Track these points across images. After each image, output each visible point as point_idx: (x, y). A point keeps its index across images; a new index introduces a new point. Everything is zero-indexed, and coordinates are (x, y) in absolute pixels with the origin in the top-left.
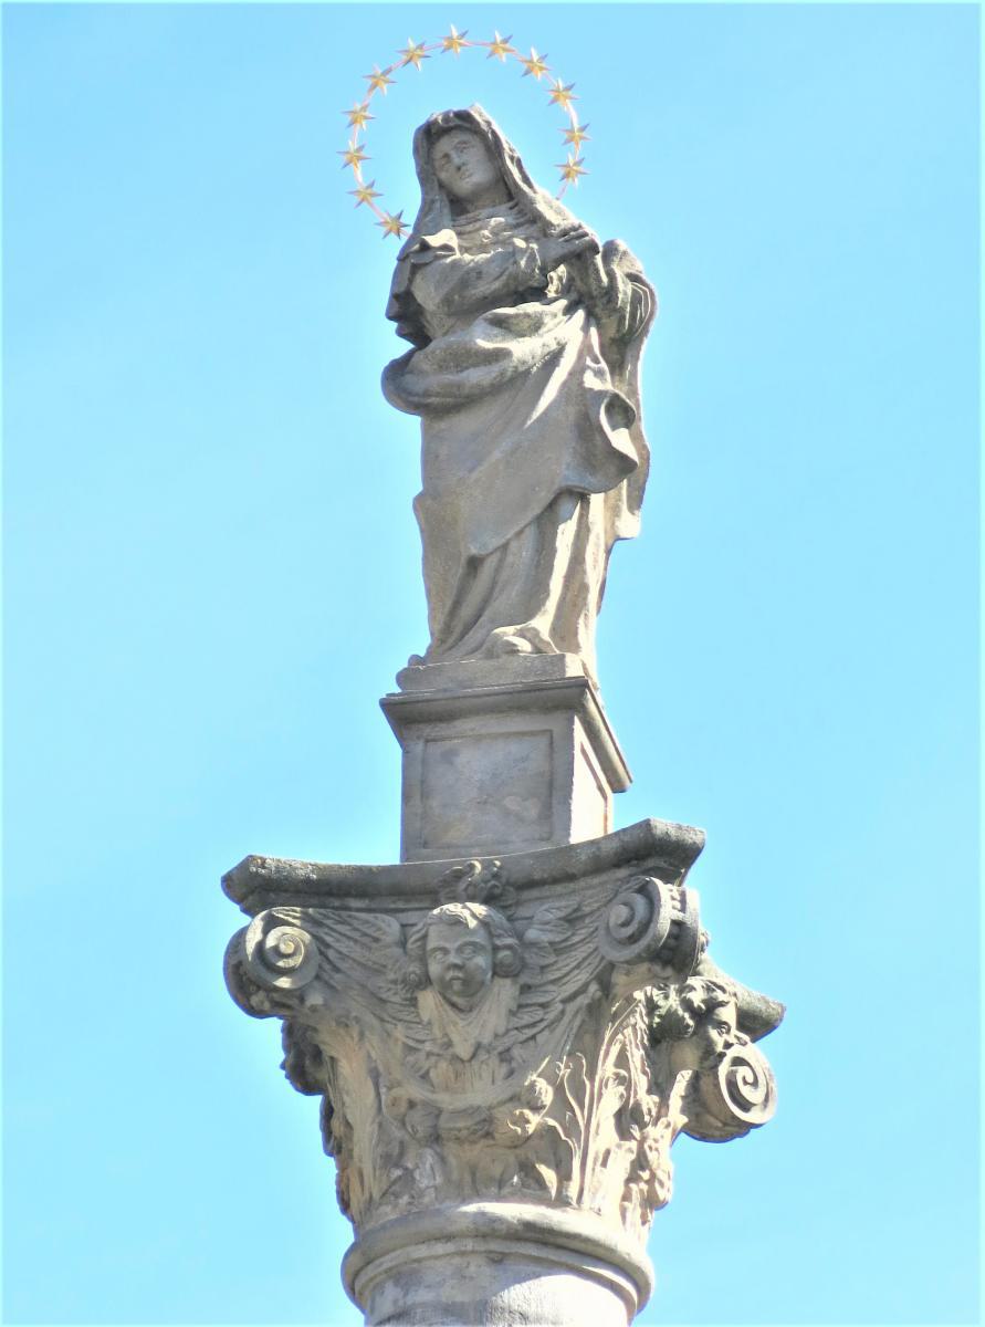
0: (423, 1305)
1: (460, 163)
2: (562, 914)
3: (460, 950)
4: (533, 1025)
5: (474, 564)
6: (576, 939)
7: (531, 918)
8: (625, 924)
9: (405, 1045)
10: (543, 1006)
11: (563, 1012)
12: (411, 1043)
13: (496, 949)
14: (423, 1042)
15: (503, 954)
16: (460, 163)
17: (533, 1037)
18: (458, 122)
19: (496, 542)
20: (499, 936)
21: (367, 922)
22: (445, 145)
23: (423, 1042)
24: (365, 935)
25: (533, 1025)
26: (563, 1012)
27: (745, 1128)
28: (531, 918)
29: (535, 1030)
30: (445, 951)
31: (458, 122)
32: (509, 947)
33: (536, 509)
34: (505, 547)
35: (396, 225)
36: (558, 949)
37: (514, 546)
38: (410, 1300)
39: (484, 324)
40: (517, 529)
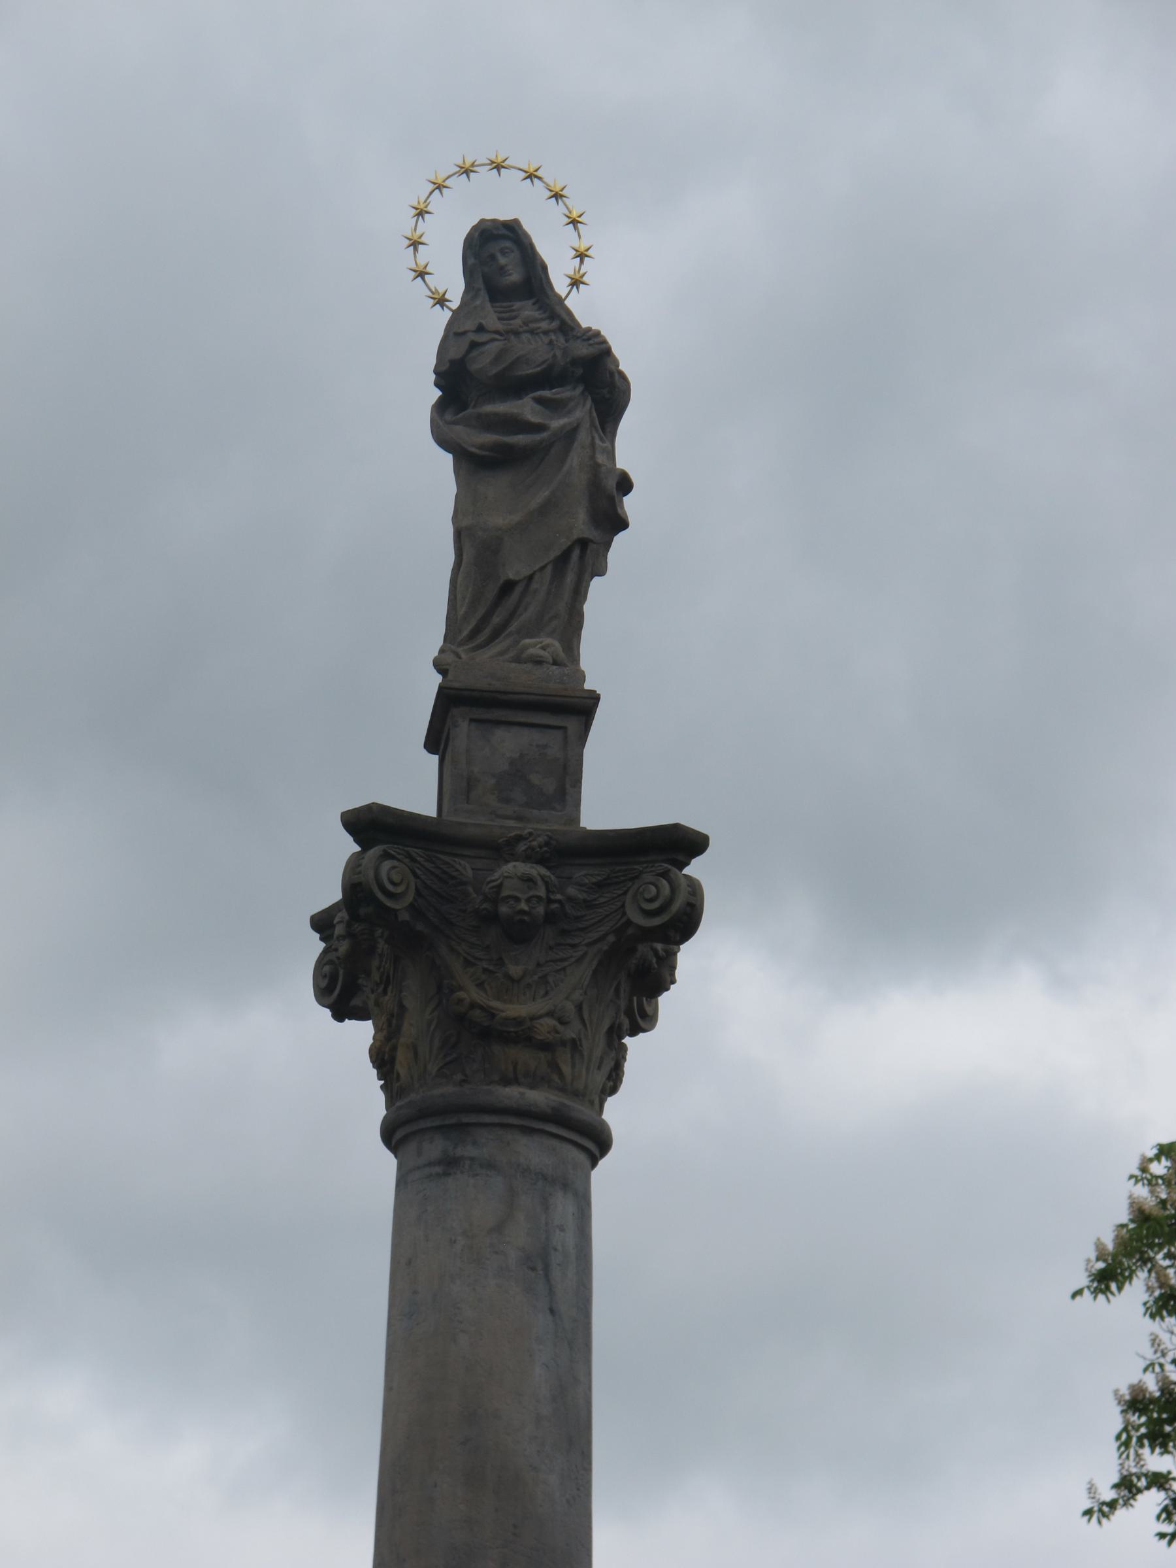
0: (472, 1159)
1: (502, 263)
2: (594, 880)
3: (528, 900)
4: (562, 960)
5: (508, 587)
6: (602, 900)
7: (570, 878)
8: (651, 900)
9: (465, 959)
10: (573, 946)
11: (585, 954)
12: (470, 958)
13: (550, 901)
14: (481, 960)
15: (555, 906)
16: (502, 263)
17: (564, 969)
18: (504, 231)
19: (526, 572)
20: (553, 892)
21: (446, 863)
22: (494, 248)
23: (481, 960)
24: (445, 872)
25: (562, 960)
26: (585, 954)
27: (1108, 1277)
28: (570, 878)
29: (566, 964)
30: (517, 900)
31: (504, 231)
32: (559, 901)
33: (555, 553)
34: (530, 578)
35: (441, 301)
36: (589, 905)
37: (537, 578)
38: (459, 1152)
39: (532, 403)
40: (542, 564)
